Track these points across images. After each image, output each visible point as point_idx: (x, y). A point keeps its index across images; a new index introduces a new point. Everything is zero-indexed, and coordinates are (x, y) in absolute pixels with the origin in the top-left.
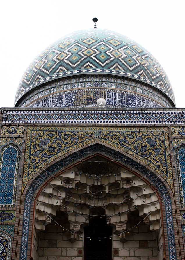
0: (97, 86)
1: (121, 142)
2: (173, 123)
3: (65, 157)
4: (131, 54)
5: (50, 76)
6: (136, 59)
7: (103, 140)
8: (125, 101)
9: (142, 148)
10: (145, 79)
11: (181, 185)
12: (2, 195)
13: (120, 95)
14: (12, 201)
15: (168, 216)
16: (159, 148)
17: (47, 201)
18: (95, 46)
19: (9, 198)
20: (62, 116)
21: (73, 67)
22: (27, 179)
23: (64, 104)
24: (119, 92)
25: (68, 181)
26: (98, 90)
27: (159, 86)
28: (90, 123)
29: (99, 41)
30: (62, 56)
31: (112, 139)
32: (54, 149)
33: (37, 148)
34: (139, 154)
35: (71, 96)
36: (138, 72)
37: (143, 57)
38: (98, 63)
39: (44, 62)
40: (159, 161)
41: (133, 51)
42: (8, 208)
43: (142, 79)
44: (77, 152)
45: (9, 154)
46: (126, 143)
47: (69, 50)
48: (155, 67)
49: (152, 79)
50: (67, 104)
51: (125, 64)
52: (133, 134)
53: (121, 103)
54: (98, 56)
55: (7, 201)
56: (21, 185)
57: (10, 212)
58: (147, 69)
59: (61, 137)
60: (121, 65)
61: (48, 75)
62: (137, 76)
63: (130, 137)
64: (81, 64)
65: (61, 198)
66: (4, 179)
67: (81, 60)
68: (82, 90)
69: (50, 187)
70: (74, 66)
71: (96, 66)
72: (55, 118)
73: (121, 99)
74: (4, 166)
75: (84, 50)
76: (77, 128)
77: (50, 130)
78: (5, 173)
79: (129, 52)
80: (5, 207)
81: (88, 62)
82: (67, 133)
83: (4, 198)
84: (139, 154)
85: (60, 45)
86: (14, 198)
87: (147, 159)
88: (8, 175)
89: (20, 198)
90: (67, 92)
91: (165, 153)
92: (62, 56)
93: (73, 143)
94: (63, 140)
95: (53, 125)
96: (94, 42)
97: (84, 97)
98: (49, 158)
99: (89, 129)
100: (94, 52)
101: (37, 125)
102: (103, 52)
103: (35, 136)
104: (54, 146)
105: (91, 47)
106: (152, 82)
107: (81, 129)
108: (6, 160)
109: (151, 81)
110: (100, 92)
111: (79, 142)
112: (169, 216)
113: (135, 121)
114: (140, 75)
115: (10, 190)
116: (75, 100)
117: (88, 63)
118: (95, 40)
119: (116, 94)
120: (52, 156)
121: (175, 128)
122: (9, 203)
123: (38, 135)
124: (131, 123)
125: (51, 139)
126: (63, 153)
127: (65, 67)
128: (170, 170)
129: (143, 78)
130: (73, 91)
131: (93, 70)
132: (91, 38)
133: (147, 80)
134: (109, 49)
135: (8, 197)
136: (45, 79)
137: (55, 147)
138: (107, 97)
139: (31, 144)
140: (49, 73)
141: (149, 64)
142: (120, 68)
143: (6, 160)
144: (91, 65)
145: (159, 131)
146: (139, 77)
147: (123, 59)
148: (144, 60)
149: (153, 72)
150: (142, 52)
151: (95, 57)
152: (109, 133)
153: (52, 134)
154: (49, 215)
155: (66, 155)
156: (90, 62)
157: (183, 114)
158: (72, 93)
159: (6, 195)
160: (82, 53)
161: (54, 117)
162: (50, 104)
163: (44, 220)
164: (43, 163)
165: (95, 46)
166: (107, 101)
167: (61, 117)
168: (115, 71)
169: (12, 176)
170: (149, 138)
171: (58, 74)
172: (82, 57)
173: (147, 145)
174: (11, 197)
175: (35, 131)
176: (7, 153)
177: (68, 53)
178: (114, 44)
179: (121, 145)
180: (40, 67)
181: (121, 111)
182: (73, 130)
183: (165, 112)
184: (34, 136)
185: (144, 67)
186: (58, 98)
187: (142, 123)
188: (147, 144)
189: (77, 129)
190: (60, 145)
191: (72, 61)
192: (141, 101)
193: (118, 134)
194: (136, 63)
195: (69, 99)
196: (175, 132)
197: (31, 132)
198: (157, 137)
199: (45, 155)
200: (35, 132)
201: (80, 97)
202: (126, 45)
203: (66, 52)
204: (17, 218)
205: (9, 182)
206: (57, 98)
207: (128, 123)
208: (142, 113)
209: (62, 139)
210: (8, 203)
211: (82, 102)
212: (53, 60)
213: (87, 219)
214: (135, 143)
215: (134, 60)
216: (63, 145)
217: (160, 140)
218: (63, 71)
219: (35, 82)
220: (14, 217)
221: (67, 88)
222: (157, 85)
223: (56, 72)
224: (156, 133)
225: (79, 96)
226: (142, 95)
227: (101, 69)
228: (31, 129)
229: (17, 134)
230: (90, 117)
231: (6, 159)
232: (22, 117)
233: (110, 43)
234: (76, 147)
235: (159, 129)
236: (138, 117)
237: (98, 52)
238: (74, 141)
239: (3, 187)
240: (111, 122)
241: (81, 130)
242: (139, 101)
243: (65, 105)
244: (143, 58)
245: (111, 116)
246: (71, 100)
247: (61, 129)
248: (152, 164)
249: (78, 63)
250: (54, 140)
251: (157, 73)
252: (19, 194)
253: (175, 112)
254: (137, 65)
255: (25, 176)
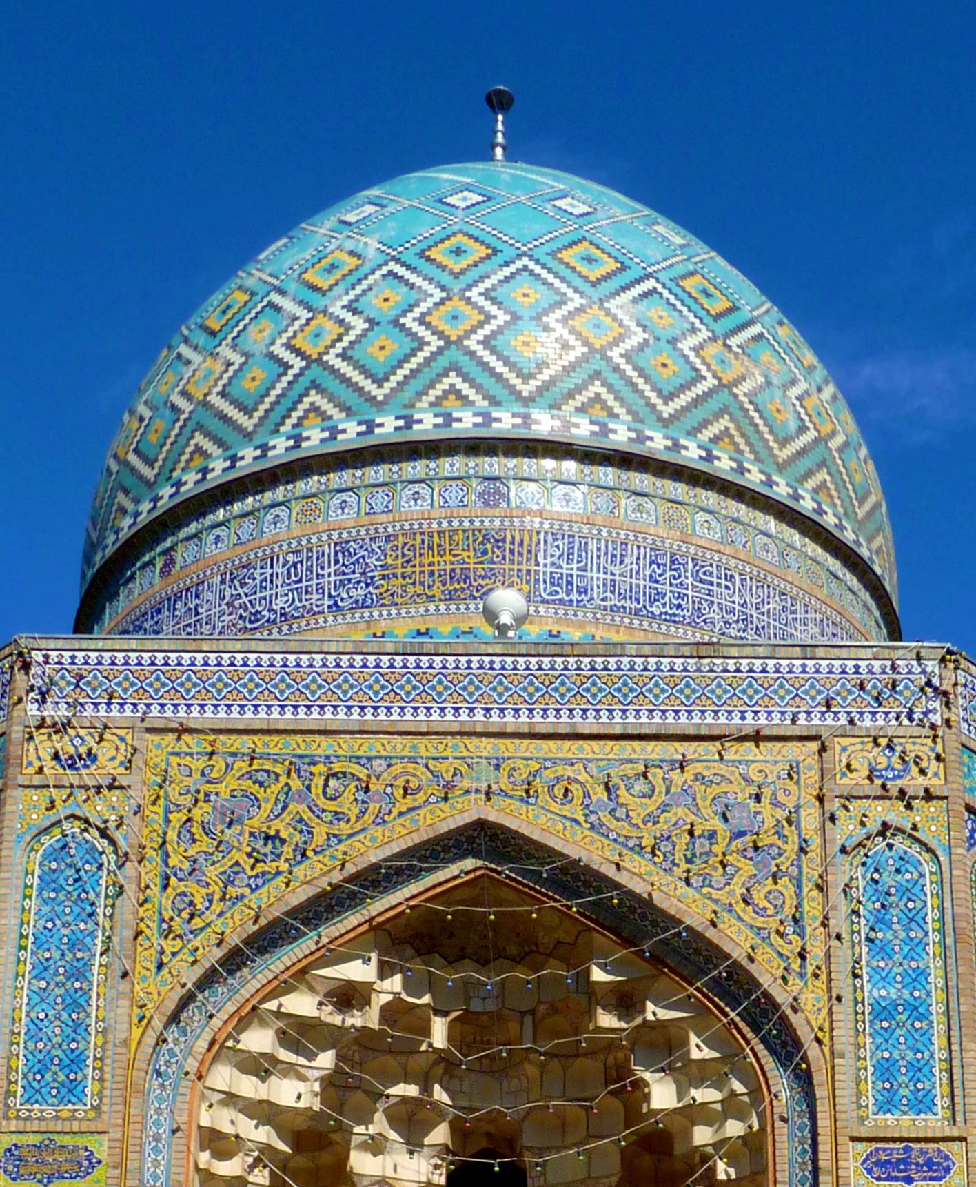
0: (496, 505)
1: (592, 812)
2: (843, 720)
3: (330, 884)
4: (672, 325)
5: (259, 443)
6: (698, 355)
7: (508, 801)
8: (634, 581)
9: (694, 843)
10: (740, 464)
11: (864, 1022)
12: (39, 1061)
13: (606, 554)
14: (88, 1091)
15: (800, 1160)
16: (772, 845)
17: (248, 1087)
18: (488, 284)
19: (72, 1076)
20: (314, 681)
21: (375, 397)
22: (152, 989)
23: (330, 596)
24: (604, 533)
25: (348, 996)
26: (497, 522)
27: (807, 496)
28: (449, 717)
29: (509, 253)
30: (317, 335)
31: (554, 798)
32: (277, 843)
33: (194, 841)
34: (678, 871)
35: (363, 557)
36: (705, 424)
37: (734, 342)
38: (499, 377)
39: (229, 364)
40: (768, 905)
41: (685, 309)
42: (67, 1123)
43: (724, 465)
44: (385, 860)
45: (63, 866)
46: (618, 819)
47: (351, 301)
48: (794, 392)
49: (778, 464)
50: (345, 595)
51: (640, 381)
52: (654, 775)
53: (613, 592)
54: (498, 342)
55: (64, 1091)
56: (126, 1018)
57: (80, 1141)
58: (751, 407)
59: (309, 788)
60: (617, 388)
61: (248, 436)
62: (699, 447)
63: (637, 788)
64: (416, 385)
65: (317, 1074)
66: (45, 990)
67: (413, 360)
68: (420, 524)
69: (263, 1023)
70: (379, 393)
71: (491, 393)
72: (282, 692)
73: (612, 574)
74: (45, 928)
75: (429, 303)
76: (385, 742)
77: (257, 750)
78: (47, 960)
79: (664, 314)
80: (57, 1118)
81: (451, 369)
82: (337, 767)
83: (48, 1077)
84: (678, 871)
85: (306, 272)
86: (93, 1078)
87: (714, 896)
88: (61, 970)
89: (123, 1078)
90: (345, 535)
91: (799, 867)
92: (317, 335)
93: (366, 816)
94: (322, 802)
95: (273, 727)
96: (482, 260)
97: (426, 562)
98: (253, 891)
99: (441, 747)
100: (482, 317)
101: (192, 725)
102: (526, 317)
103: (189, 781)
104: (278, 831)
105: (465, 290)
106: (775, 478)
107: (407, 749)
108: (53, 895)
109: (768, 470)
110: (508, 533)
111: (395, 812)
112: (804, 1163)
113: (664, 712)
114: (716, 439)
115: (74, 1040)
116: (383, 577)
117: (447, 376)
118: (488, 247)
119: (586, 544)
120: (269, 880)
121: (851, 749)
122: (74, 1099)
123: (197, 776)
124: (644, 720)
125: (261, 794)
126: (321, 866)
127: (332, 394)
128: (816, 954)
129: (731, 459)
130: (376, 529)
131: (475, 415)
132: (466, 234)
133: (746, 465)
134: (558, 298)
135: (67, 1071)
136: (234, 459)
137: (283, 835)
138: (541, 559)
139: (168, 821)
140: (255, 426)
141: (760, 379)
142: (612, 408)
143: (54, 899)
144: (465, 388)
145: (776, 762)
146: (709, 451)
147: (627, 356)
148: (736, 354)
149: (784, 423)
150: (732, 310)
151: (486, 342)
152: (537, 766)
153: (267, 772)
154: (261, 1151)
155: (336, 877)
156: (460, 373)
157: (899, 673)
158: (367, 541)
159: (56, 1061)
160: (421, 321)
161: (276, 686)
162: (259, 595)
163: (238, 1173)
164: (228, 915)
165: (488, 284)
166: (545, 582)
167: (307, 687)
168: (587, 421)
169: (80, 973)
170: (726, 793)
171: (297, 431)
172: (422, 344)
173: (715, 832)
174: (80, 1074)
175: (187, 754)
176: (54, 865)
177: (348, 316)
178: (585, 271)
179: (592, 827)
180: (206, 390)
181: (599, 660)
182: (368, 754)
183: (810, 663)
184: (182, 781)
185: (735, 396)
186: (301, 562)
187: (696, 720)
188: (717, 824)
189: (388, 748)
190: (306, 824)
191: (369, 364)
192: (715, 580)
193: (583, 777)
194: (694, 374)
195: (354, 572)
196: (854, 765)
197: (168, 764)
198: (767, 792)
199: (236, 873)
200: (182, 762)
201: (408, 562)
202: (649, 276)
203: (337, 309)
204: (115, 1167)
205: (69, 1001)
206: (295, 565)
207: (631, 720)
208: (698, 670)
209: (317, 795)
210: (69, 1101)
211: (419, 589)
212: (272, 356)
213: (436, 1167)
214: (661, 820)
215: (685, 357)
216: (318, 824)
217: (776, 804)
218: (325, 417)
219: (183, 470)
220: (99, 1162)
221: (343, 509)
222: (800, 492)
223: (289, 422)
224: (760, 771)
225: (404, 555)
226: (719, 552)
227: (516, 410)
228: (164, 744)
229: (99, 771)
230: (446, 688)
231: (54, 890)
232: (119, 684)
233: (567, 265)
234: (379, 834)
235: (776, 750)
236: (681, 691)
237: (502, 318)
238: (372, 806)
239: (40, 1025)
240: (552, 713)
241: (404, 753)
242: (701, 581)
243: (336, 604)
244: (735, 349)
245: (551, 683)
246: (363, 573)
247: (308, 745)
248: (733, 921)
249: (401, 374)
250: (277, 799)
251: (803, 429)
252: (116, 1057)
253: (857, 667)
254: (700, 388)
255: (144, 972)
